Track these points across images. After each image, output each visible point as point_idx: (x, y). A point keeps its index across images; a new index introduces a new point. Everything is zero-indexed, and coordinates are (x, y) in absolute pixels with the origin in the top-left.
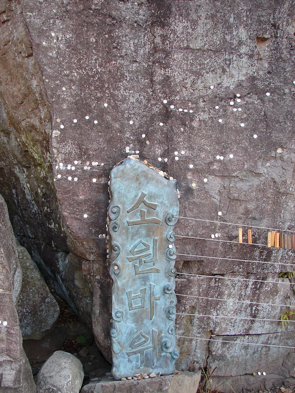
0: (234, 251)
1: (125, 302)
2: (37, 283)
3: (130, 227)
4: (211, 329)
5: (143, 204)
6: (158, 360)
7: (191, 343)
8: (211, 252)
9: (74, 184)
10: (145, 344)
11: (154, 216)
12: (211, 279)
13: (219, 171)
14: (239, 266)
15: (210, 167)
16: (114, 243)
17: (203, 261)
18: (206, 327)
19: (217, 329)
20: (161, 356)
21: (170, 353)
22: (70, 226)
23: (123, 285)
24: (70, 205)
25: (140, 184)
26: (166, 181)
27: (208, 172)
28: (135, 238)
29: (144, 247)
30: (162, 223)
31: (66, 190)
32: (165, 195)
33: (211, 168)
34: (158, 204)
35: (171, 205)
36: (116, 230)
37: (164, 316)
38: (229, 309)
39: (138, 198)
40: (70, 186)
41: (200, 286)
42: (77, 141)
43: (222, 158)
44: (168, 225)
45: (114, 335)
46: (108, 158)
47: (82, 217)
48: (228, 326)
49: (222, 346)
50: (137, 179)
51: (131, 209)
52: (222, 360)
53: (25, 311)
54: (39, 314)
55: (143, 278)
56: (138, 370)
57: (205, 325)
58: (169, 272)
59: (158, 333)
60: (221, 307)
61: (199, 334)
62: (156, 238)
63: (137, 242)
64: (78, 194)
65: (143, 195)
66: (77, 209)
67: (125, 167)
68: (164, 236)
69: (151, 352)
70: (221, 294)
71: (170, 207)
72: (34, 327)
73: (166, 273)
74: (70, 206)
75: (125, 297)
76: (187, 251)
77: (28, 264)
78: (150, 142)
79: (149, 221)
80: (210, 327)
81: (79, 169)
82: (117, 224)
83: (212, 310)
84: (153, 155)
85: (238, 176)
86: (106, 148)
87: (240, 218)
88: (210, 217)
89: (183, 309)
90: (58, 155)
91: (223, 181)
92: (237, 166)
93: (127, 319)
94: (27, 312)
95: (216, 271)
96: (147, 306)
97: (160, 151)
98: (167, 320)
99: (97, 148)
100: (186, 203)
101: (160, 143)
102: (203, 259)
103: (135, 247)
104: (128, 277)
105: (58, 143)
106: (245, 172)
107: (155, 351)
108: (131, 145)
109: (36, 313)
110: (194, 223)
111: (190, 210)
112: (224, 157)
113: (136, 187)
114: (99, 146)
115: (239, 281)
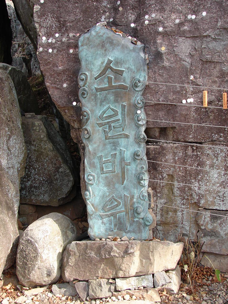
0: (211, 117)
1: (97, 166)
2: (50, 153)
3: (98, 93)
4: (195, 201)
5: (109, 70)
6: (131, 225)
7: (176, 214)
8: (183, 118)
9: (54, 56)
10: (118, 208)
11: (122, 82)
12: (187, 147)
13: (190, 31)
14: (218, 134)
15: (180, 28)
16: (84, 109)
17: (175, 127)
18: (189, 198)
19: (202, 202)
20: (134, 221)
21: (143, 219)
22: (52, 95)
23: (94, 150)
24: (51, 75)
25: (105, 50)
26: (131, 46)
27: (178, 33)
28: (104, 103)
29: (113, 113)
30: (130, 88)
31: (46, 61)
32: (131, 60)
33: (181, 29)
34: (124, 70)
35: (138, 70)
36: (84, 96)
37: (135, 182)
38: (213, 181)
39: (105, 64)
40: (50, 58)
41: (175, 154)
42: (56, 14)
43: (194, 17)
44: (135, 90)
45: (87, 197)
46: (84, 28)
47: (62, 86)
48: (216, 200)
49: (212, 220)
50: (103, 46)
51: (98, 75)
52: (215, 237)
53: (42, 179)
54: (55, 182)
55: (114, 143)
56: (111, 233)
57: (187, 196)
58: (139, 138)
59: (130, 199)
60: (202, 178)
61: (184, 205)
62: (124, 104)
63: (105, 108)
64: (57, 65)
65: (110, 62)
66: (57, 79)
67: (91, 34)
68: (132, 101)
69: (124, 216)
70: (201, 164)
71: (137, 72)
72: (51, 194)
73: (136, 139)
74: (51, 77)
75: (96, 161)
76: (160, 118)
77: (42, 136)
78: (123, 8)
79: (116, 87)
80: (193, 198)
81: (59, 41)
82: (85, 91)
83: (193, 181)
84: (126, 22)
85: (209, 36)
86: (82, 19)
87: (215, 82)
88: (181, 81)
89: (160, 177)
90: (40, 29)
91: (194, 42)
92: (209, 24)
93: (99, 182)
94: (44, 180)
95: (190, 138)
96: (118, 170)
97: (133, 16)
98: (139, 186)
99: (74, 20)
100: (155, 68)
101: (134, 8)
102: (174, 125)
103: (104, 112)
104: (98, 142)
105: (39, 17)
106: (218, 30)
107: (128, 215)
108: (107, 14)
109: (52, 182)
110: (164, 88)
111: (160, 75)
112: (196, 15)
113: (103, 54)
114: (76, 17)
115: (222, 151)
